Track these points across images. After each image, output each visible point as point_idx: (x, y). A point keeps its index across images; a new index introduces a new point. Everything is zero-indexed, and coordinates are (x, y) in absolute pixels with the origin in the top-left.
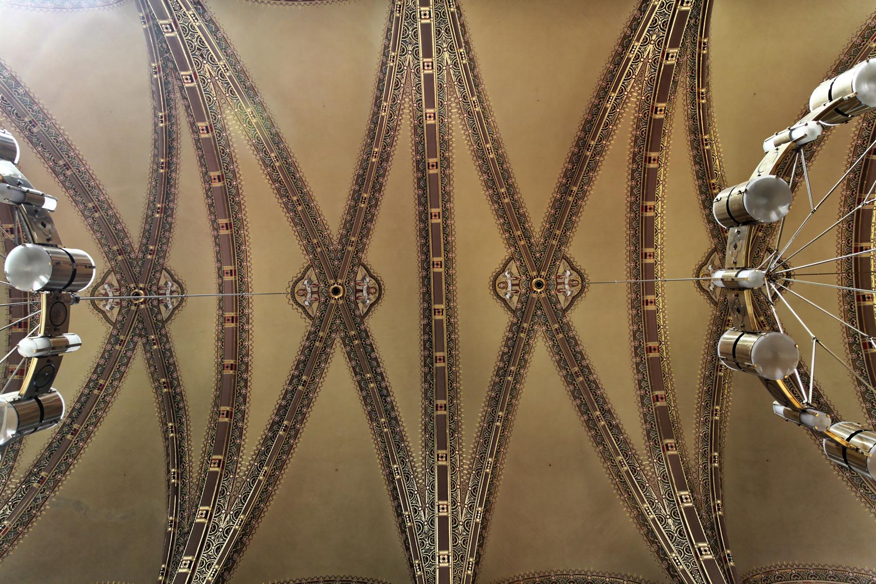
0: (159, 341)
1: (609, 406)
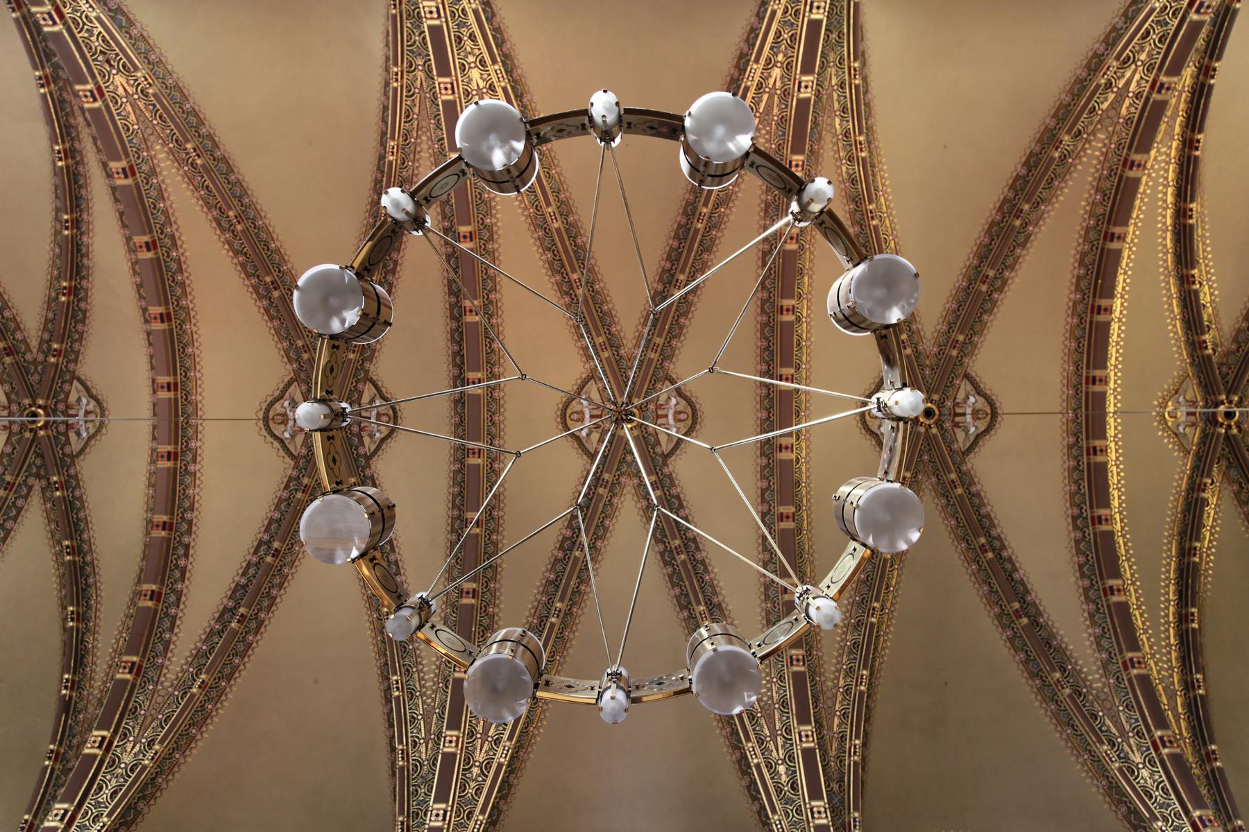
0: (63, 486)
1: (720, 598)
